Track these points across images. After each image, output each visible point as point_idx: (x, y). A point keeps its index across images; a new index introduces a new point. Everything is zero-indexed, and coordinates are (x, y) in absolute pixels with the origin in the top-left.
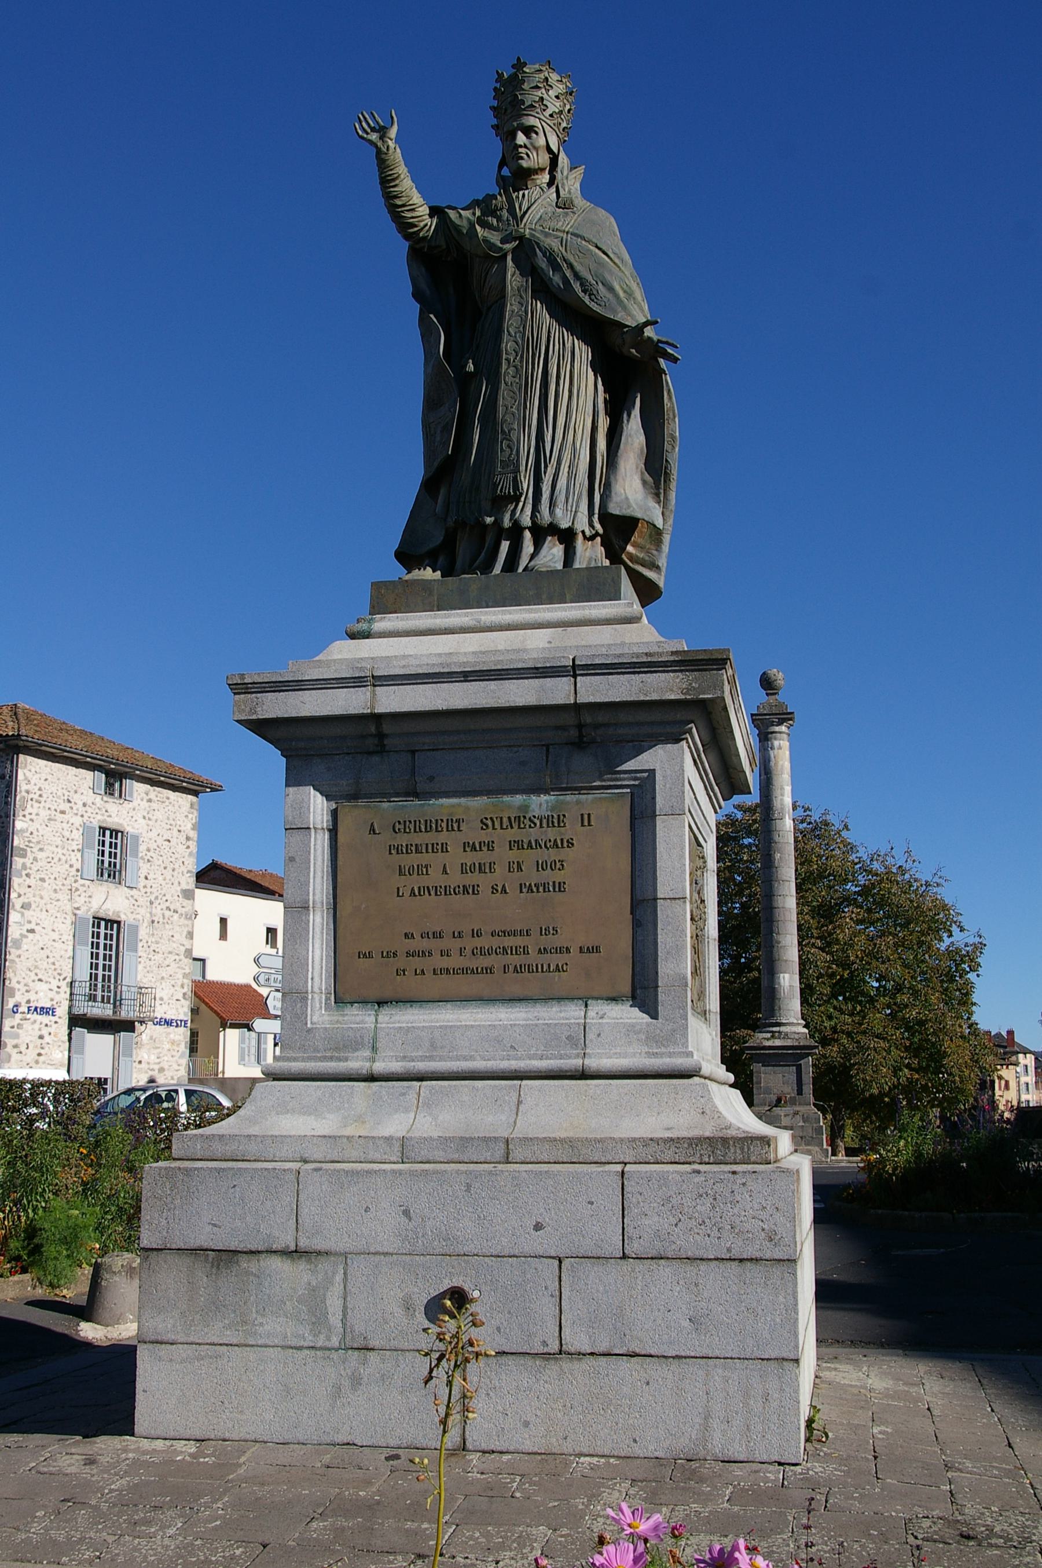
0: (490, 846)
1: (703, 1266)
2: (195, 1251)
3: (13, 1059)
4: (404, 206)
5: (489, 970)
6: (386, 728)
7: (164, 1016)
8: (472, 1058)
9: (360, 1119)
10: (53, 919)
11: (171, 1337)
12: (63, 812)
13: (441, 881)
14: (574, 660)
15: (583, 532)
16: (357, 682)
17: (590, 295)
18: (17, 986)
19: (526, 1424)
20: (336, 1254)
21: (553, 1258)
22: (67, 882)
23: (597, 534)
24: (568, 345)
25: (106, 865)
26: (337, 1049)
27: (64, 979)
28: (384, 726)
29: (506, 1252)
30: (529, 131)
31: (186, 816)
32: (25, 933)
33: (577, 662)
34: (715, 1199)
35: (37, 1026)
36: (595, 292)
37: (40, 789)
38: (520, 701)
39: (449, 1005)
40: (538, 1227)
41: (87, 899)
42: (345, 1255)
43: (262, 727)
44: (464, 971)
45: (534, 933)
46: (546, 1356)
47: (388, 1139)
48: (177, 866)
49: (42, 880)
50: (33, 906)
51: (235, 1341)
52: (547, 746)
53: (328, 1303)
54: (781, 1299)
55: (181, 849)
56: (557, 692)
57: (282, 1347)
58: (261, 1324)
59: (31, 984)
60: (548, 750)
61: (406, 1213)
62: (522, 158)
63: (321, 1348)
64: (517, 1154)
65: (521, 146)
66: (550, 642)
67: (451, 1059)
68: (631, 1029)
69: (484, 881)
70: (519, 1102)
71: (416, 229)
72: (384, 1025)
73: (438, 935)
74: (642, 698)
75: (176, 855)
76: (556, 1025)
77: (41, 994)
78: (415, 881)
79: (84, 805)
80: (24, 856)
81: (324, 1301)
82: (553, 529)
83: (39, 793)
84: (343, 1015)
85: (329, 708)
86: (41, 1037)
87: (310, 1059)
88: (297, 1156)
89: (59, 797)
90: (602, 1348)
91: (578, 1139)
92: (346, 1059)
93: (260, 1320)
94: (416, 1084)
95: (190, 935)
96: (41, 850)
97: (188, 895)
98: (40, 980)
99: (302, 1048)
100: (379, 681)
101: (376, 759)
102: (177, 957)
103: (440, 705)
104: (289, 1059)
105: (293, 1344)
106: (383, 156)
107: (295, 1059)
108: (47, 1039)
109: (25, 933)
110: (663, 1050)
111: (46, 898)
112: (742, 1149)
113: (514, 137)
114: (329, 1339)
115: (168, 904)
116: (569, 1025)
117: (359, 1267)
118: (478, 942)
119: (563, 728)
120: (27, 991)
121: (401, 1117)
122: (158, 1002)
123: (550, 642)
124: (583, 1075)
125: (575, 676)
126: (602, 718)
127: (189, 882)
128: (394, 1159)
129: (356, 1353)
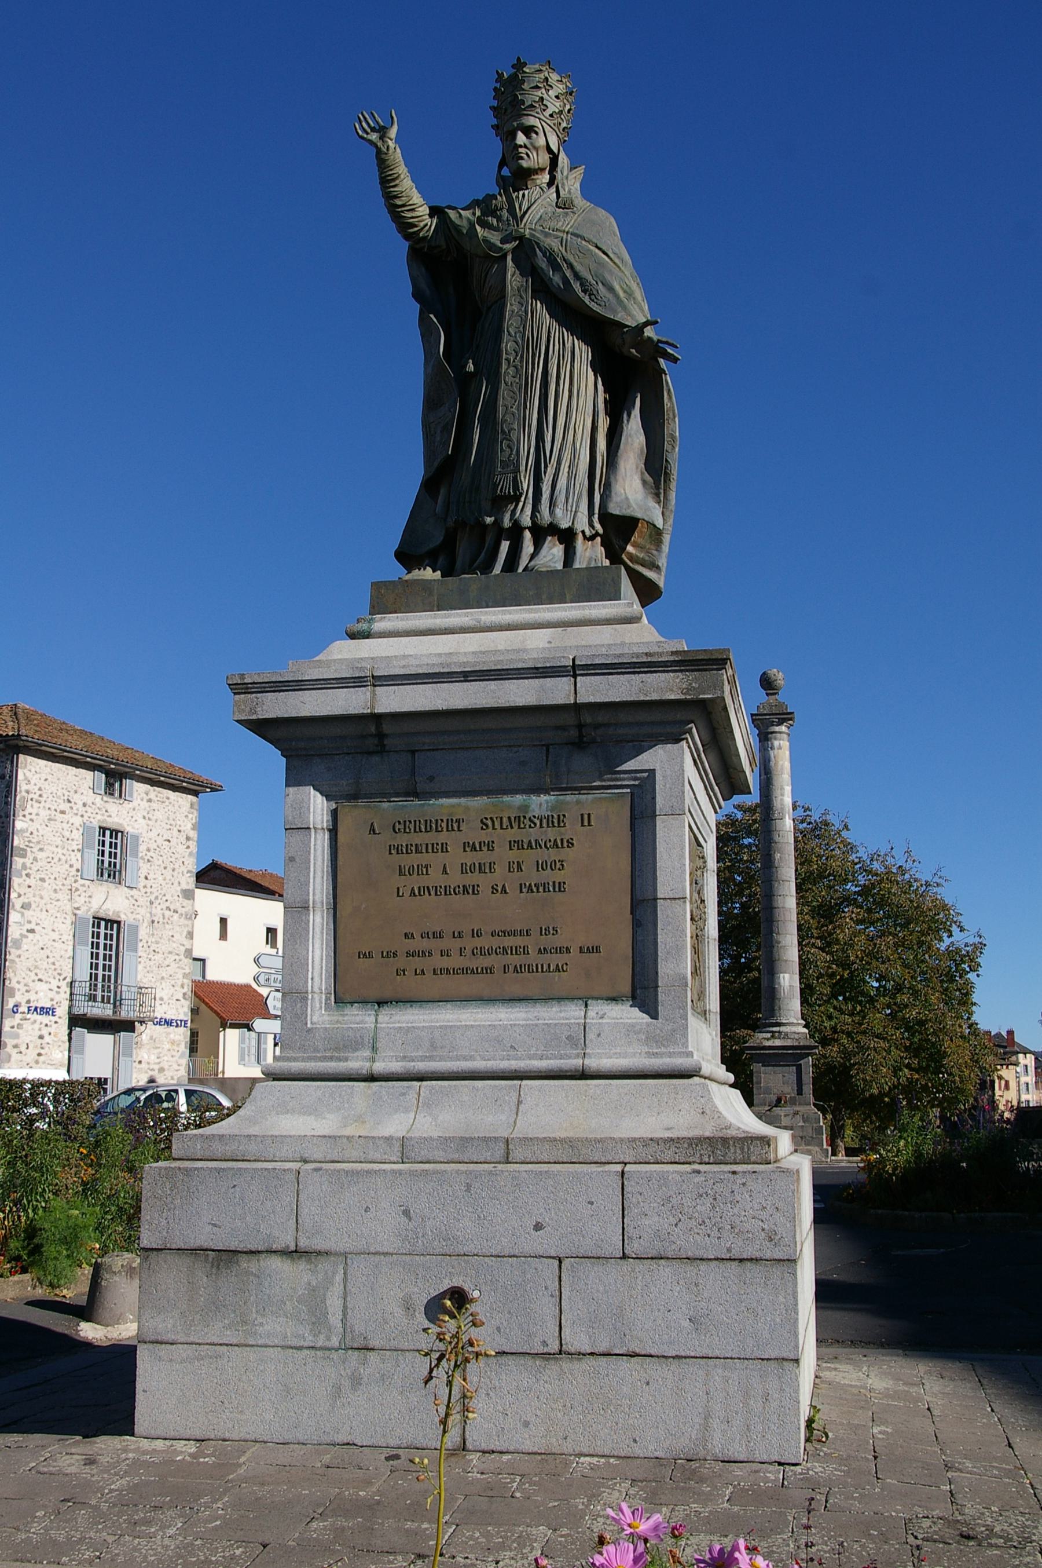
0: (490, 846)
1: (703, 1266)
2: (195, 1251)
3: (13, 1059)
4: (404, 206)
5: (489, 970)
6: (387, 728)
7: (164, 1016)
8: (472, 1058)
9: (360, 1119)
10: (53, 919)
11: (171, 1337)
12: (63, 812)
13: (441, 880)
14: (574, 660)
15: (583, 532)
16: (356, 682)
17: (590, 295)
18: (17, 986)
19: (526, 1424)
20: (337, 1254)
21: (553, 1258)
22: (67, 882)
23: (597, 534)
24: (568, 345)
25: (106, 864)
26: (337, 1049)
27: (64, 979)
28: (384, 726)
29: (506, 1252)
30: (529, 131)
31: (186, 816)
32: (25, 933)
33: (577, 662)
34: (715, 1199)
35: (37, 1026)
36: (595, 292)
37: (40, 789)
38: (520, 701)
39: (449, 1005)
40: (538, 1227)
41: (87, 899)
42: (345, 1255)
43: (262, 727)
44: (464, 971)
45: (534, 932)
46: (546, 1356)
47: (388, 1139)
48: (177, 866)
49: (43, 880)
50: (33, 906)
51: (235, 1341)
52: (547, 746)
53: (328, 1303)
54: (781, 1299)
55: (181, 849)
56: (557, 692)
57: (282, 1347)
58: (261, 1324)
59: (31, 984)
60: (548, 751)
61: (406, 1213)
62: (522, 158)
63: (321, 1348)
64: (517, 1154)
65: (521, 146)
66: (550, 642)
67: (451, 1059)
68: (631, 1029)
69: (484, 881)
70: (519, 1102)
71: (416, 229)
72: (383, 1025)
73: (438, 935)
74: (642, 698)
75: (176, 855)
76: (556, 1025)
77: (41, 994)
78: (416, 881)
79: (84, 805)
80: (24, 856)
81: (324, 1301)
82: (553, 529)
83: (39, 793)
84: (343, 1015)
85: (329, 708)
86: (41, 1037)
87: (310, 1059)
88: (297, 1156)
89: (59, 797)
90: (602, 1348)
91: (578, 1139)
92: (346, 1059)
93: (260, 1320)
94: (416, 1084)
95: (190, 935)
96: (41, 850)
97: (188, 895)
98: (40, 980)
99: (302, 1048)
100: (379, 681)
101: (376, 759)
102: (177, 957)
103: (440, 705)
104: (289, 1059)
105: (293, 1344)
106: (383, 156)
107: (295, 1059)
108: (47, 1039)
109: (25, 933)
110: (663, 1050)
111: (46, 898)
112: (742, 1149)
113: (514, 137)
114: (329, 1339)
115: (168, 904)
116: (569, 1025)
117: (359, 1267)
118: (478, 942)
119: (563, 728)
120: (27, 991)
121: (401, 1117)
122: (158, 1002)
123: (550, 642)
124: (583, 1075)
125: (575, 676)
126: (602, 718)
127: (189, 882)
128: (394, 1159)
129: (356, 1353)
